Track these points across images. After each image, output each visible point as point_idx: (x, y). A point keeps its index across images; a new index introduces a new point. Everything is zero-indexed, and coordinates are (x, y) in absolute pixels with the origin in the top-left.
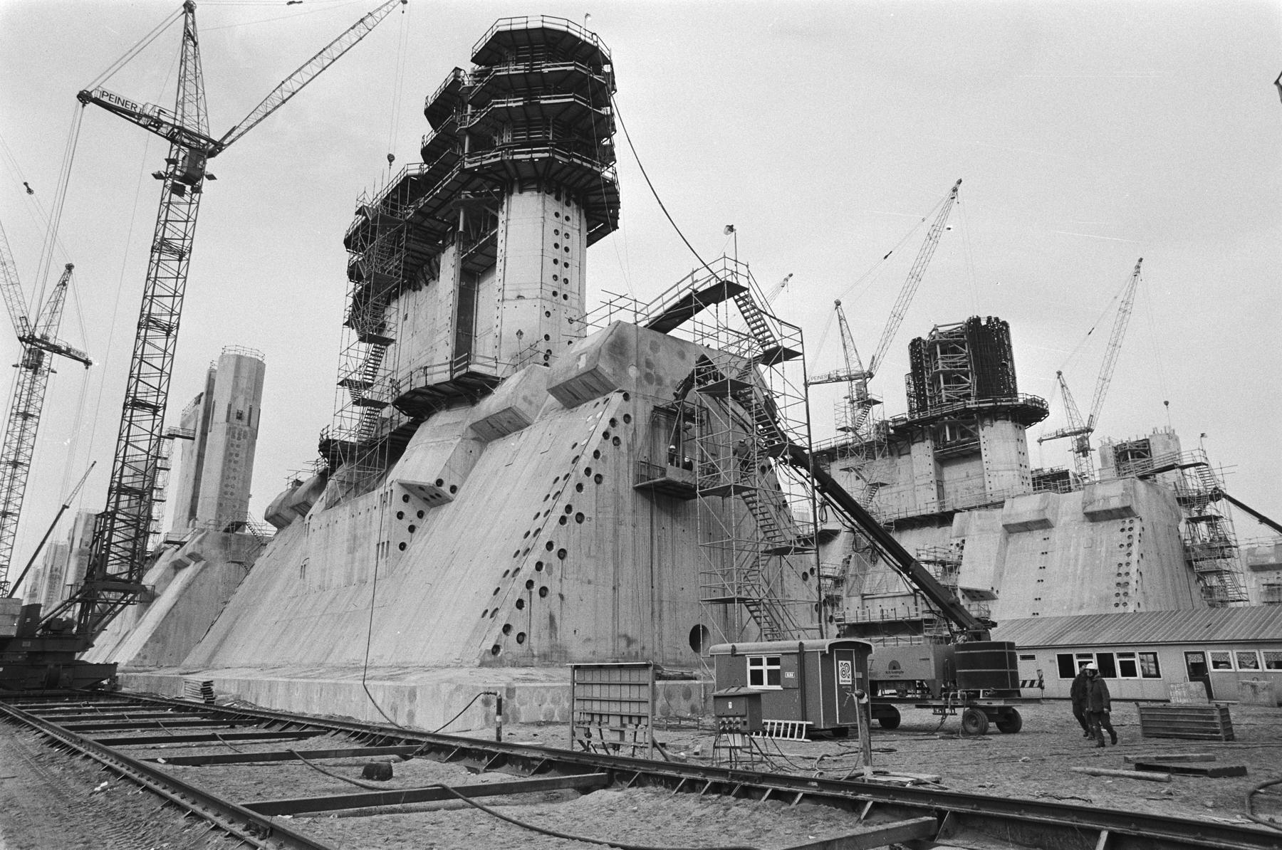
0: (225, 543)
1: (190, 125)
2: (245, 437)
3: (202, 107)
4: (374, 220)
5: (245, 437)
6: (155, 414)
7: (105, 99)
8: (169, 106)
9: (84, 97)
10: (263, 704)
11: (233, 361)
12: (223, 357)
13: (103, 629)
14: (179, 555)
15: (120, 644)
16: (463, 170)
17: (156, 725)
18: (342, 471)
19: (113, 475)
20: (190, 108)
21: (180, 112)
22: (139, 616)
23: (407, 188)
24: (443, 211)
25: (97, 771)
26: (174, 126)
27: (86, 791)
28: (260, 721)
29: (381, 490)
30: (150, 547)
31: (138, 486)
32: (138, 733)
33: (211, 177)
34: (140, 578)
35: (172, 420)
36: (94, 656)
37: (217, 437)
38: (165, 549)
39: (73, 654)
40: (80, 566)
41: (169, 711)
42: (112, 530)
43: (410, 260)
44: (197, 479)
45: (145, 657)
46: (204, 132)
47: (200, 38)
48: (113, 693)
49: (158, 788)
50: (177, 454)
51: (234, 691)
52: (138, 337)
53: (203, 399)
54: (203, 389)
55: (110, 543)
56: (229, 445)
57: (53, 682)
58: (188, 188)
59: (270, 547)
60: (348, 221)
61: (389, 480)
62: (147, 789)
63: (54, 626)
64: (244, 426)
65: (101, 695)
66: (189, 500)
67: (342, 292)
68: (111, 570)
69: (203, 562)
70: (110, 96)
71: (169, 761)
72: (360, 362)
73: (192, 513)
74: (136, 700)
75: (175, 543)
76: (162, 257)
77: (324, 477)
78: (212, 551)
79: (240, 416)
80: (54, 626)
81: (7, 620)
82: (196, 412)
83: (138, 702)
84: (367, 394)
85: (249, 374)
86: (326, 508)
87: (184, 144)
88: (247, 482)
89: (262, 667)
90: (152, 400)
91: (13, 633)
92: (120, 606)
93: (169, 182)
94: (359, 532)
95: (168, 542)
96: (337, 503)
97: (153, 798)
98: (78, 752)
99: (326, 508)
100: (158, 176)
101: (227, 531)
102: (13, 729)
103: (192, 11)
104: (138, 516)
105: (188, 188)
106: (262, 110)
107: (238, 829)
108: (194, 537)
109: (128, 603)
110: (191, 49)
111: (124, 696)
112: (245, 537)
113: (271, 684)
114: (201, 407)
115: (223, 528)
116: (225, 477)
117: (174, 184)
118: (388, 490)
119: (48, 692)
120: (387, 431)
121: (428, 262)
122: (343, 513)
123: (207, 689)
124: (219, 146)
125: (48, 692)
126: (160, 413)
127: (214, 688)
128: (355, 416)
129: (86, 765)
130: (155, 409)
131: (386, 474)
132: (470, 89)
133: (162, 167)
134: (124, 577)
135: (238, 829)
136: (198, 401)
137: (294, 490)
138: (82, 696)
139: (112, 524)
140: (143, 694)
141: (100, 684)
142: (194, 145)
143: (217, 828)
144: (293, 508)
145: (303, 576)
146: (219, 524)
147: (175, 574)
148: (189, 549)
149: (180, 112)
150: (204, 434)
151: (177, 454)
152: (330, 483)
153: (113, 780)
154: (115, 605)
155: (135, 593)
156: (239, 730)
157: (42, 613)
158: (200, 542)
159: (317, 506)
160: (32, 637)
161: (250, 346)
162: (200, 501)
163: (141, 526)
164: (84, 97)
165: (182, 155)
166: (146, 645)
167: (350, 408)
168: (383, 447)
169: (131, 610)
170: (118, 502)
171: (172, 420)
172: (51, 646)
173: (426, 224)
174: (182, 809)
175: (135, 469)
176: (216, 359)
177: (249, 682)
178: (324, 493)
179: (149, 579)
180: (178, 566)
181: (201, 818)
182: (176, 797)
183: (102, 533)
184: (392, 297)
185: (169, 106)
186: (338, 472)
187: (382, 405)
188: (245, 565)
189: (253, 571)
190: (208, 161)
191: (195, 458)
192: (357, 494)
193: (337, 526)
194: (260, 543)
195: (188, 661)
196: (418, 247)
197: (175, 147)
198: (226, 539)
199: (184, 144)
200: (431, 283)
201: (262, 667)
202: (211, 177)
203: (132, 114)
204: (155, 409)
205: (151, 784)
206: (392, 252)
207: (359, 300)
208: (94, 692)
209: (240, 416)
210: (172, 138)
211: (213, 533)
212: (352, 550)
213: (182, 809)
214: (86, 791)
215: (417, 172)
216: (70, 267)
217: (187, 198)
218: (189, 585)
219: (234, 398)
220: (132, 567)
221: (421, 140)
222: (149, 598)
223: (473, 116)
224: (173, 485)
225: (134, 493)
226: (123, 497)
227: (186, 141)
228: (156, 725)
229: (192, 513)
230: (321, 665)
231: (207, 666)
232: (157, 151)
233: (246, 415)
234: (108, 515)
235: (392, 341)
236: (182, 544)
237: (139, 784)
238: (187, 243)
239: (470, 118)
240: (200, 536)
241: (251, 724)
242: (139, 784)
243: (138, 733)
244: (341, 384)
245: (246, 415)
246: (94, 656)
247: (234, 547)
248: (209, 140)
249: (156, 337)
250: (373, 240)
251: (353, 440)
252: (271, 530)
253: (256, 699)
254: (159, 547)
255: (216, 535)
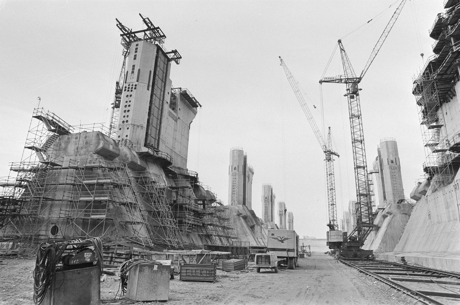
0: (399, 207)
1: (350, 77)
2: (396, 169)
3: (352, 69)
4: (421, 84)
5: (396, 169)
6: (364, 169)
7: (326, 80)
8: (342, 73)
9: (321, 82)
10: (425, 266)
11: (385, 144)
12: (381, 143)
13: (365, 239)
14: (384, 213)
15: (372, 243)
16: (453, 53)
17: (388, 270)
18: (435, 177)
19: (357, 191)
20: (348, 71)
21: (346, 73)
22: (376, 234)
23: (432, 66)
24: (449, 70)
25: (373, 279)
26: (345, 79)
27: (372, 283)
28: (423, 271)
29: (453, 184)
30: (374, 211)
31: (365, 193)
32: (383, 271)
33: (361, 89)
34: (373, 222)
35: (370, 168)
36: (365, 247)
37: (387, 171)
38: (379, 211)
39: (359, 247)
40: (354, 218)
41: (392, 266)
42: (361, 208)
43: (440, 92)
44: (383, 186)
45: (381, 248)
46: (355, 77)
47: (345, 49)
48: (373, 259)
49: (389, 283)
50: (375, 178)
51: (413, 261)
52: (353, 146)
53: (378, 158)
54: (377, 155)
55: (361, 212)
56: (391, 173)
57: (356, 256)
58: (355, 95)
59: (415, 208)
60: (412, 87)
61: (455, 179)
62: (386, 283)
63: (352, 239)
64: (395, 165)
65: (370, 260)
66: (382, 193)
67: (417, 112)
68: (364, 220)
69: (392, 215)
70: (327, 78)
71: (392, 279)
72: (431, 136)
73: (385, 198)
74: (381, 262)
75: (381, 209)
76: (353, 119)
77: (429, 180)
78: (394, 210)
79: (392, 162)
80: (352, 239)
81: (340, 237)
82: (377, 163)
83: (382, 263)
84: (439, 148)
85: (392, 147)
86: (433, 192)
87: (350, 83)
88: (401, 185)
89: (423, 252)
90: (362, 165)
91: (342, 241)
92: (369, 232)
93: (349, 96)
94: (448, 200)
95: (379, 209)
96: (436, 190)
97: (388, 286)
98: (368, 274)
99: (433, 192)
100: (345, 95)
101: (398, 203)
102: (350, 268)
103: (340, 42)
104: (367, 202)
105: (355, 95)
106: (370, 61)
107: (409, 293)
108: (387, 206)
109: (371, 231)
110: (343, 53)
111: (377, 261)
112: (405, 204)
113: (426, 259)
114: (378, 161)
115: (397, 202)
116: (393, 184)
117: (351, 96)
118: (456, 183)
119: (355, 258)
120: (450, 160)
121: (450, 90)
122: (440, 194)
123: (403, 259)
124: (360, 79)
125: (355, 258)
126: (366, 168)
127: (406, 259)
128: (434, 156)
129: (370, 278)
130: (364, 168)
131: (453, 178)
132: (448, 19)
133: (346, 92)
134: (368, 222)
135: (409, 293)
136: (377, 159)
137: (419, 186)
138: (365, 260)
139: (360, 206)
140: (383, 261)
141: (368, 256)
142: (353, 81)
143: (404, 293)
144: (420, 193)
145: (430, 218)
146: (395, 201)
147: (384, 219)
148: (386, 210)
149: (346, 73)
150: (382, 170)
151: (375, 178)
152: (431, 183)
153: (378, 281)
154: (367, 231)
155: (372, 227)
156: (416, 273)
157: (348, 235)
158: (390, 208)
159: (429, 192)
160: (347, 242)
161: (389, 137)
162: (386, 194)
163: (369, 205)
164: (321, 82)
165: (350, 86)
166: (380, 244)
167: (432, 154)
168: (450, 166)
169: (373, 233)
170: (360, 199)
171: (370, 168)
172: (353, 244)
173: (443, 77)
174: (395, 288)
175: (363, 188)
176: (379, 144)
177: (418, 258)
178: (430, 187)
179: (376, 222)
180: (385, 217)
181: (400, 291)
182: (393, 286)
183: (358, 209)
184: (437, 109)
185: (342, 73)
186: (433, 178)
187: (445, 151)
188: (408, 215)
189: (411, 217)
190: (358, 84)
191: (381, 179)
192: (444, 186)
193: (439, 198)
194: (411, 206)
195: (396, 249)
196: (443, 87)
197: (348, 85)
198: (399, 206)
199: (350, 83)
200: (454, 98)
201: (423, 252)
202: (361, 89)
203: (333, 81)
204: (364, 168)
205: (387, 282)
206: (432, 93)
207: (425, 112)
208: (368, 259)
209: (392, 162)
210: (346, 83)
211: (393, 204)
212: (447, 207)
213: (395, 288)
214: (372, 283)
215: (433, 59)
216: (329, 128)
217: (355, 99)
218: (389, 224)
219: (388, 156)
220: (369, 219)
221: (415, 100)
222: (378, 228)
223: (452, 28)
224: (376, 189)
225: (365, 195)
226: (362, 197)
227: (350, 81)
228: (388, 270)
229: (385, 198)
230: (445, 252)
231: (402, 251)
232: (343, 88)
233: (394, 161)
234: (359, 203)
235: (442, 125)
236: (384, 209)
237: (384, 282)
238: (359, 113)
239: (451, 30)
240: (389, 206)
241: (420, 272)
242: (384, 282)
243: (383, 271)
244: (426, 146)
245: (394, 161)
246: (365, 247)
247: (402, 209)
248: (357, 78)
249: (358, 138)
250: (422, 91)
251: (436, 165)
252: (414, 201)
253: (422, 264)
254: (376, 211)
255: (395, 205)
